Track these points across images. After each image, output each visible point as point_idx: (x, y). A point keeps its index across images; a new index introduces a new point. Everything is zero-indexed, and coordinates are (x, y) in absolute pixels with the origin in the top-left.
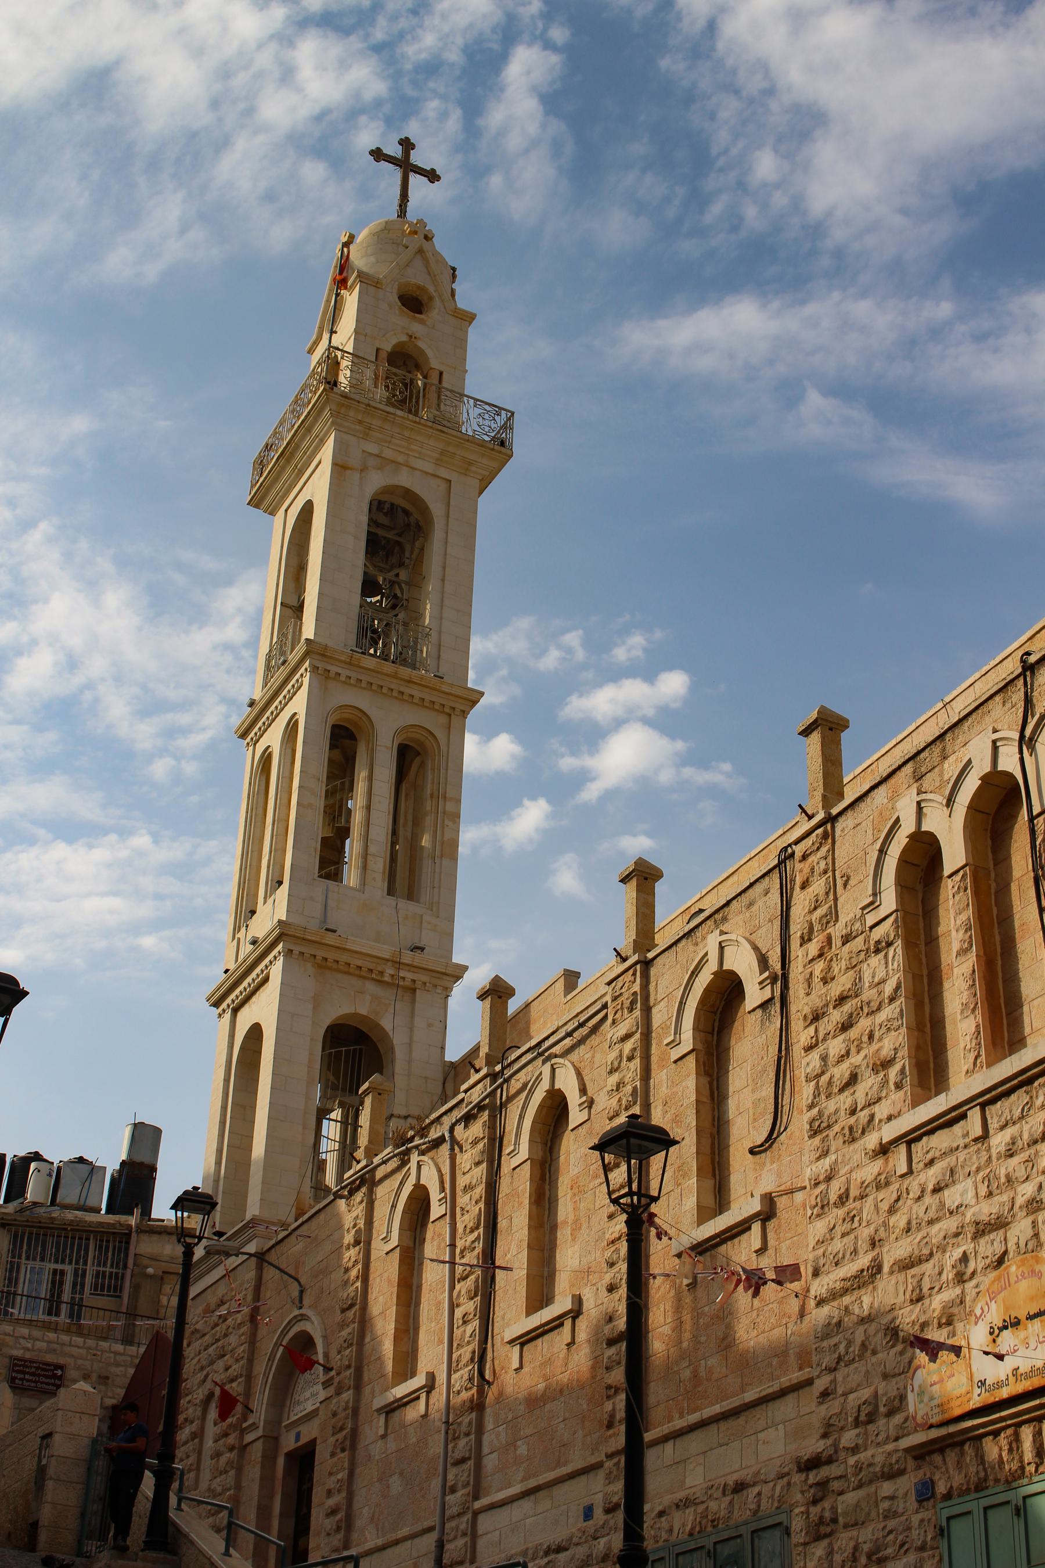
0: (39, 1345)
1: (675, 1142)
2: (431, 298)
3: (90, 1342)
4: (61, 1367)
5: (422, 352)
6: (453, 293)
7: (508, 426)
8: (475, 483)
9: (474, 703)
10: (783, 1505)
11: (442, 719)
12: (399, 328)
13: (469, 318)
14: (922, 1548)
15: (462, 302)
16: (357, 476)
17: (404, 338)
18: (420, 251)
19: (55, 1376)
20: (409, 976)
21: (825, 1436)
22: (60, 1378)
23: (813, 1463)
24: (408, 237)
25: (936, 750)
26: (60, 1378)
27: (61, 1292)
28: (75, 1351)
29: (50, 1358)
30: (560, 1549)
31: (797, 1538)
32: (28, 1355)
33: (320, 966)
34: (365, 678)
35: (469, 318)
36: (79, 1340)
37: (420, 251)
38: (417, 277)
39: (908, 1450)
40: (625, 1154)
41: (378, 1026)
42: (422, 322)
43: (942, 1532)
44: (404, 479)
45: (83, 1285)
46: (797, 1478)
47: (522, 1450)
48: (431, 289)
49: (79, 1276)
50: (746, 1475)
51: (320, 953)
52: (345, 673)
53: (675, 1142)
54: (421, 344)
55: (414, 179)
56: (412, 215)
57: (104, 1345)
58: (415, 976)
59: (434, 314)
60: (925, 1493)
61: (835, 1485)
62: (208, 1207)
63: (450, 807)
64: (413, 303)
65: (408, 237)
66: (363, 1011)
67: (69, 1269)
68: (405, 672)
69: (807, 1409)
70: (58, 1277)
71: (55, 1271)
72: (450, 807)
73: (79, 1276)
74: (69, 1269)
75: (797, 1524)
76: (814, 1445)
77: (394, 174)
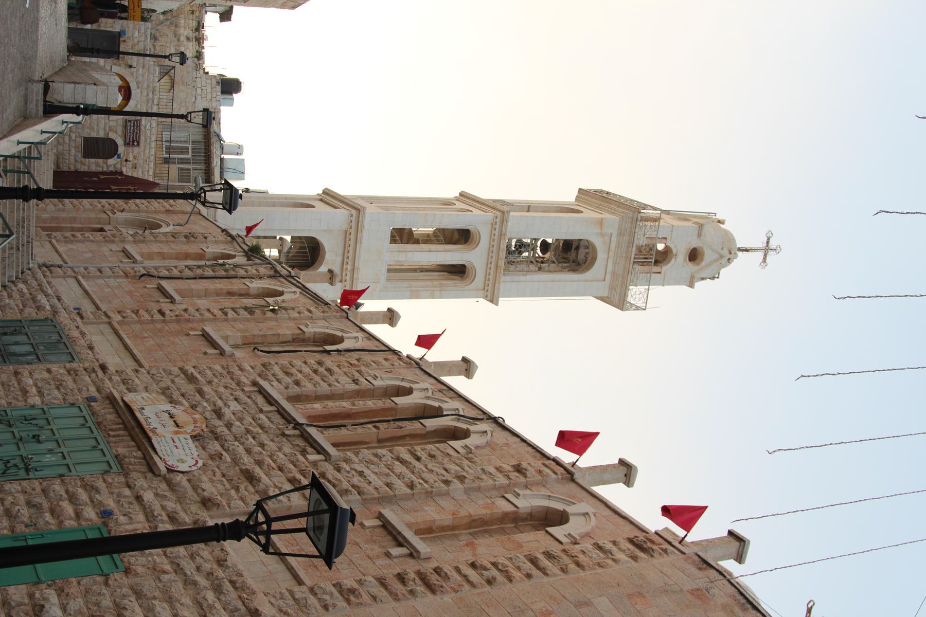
0: (148, 133)
1: (329, 564)
2: (698, 264)
3: (152, 158)
4: (138, 144)
5: (669, 262)
6: (703, 279)
7: (638, 308)
8: (605, 294)
9: (492, 301)
10: (81, 360)
11: (481, 286)
12: (681, 251)
13: (691, 285)
14: (64, 399)
15: (698, 284)
16: (598, 231)
17: (674, 252)
18: (722, 257)
19: (134, 141)
20: (348, 278)
21: (117, 371)
22: (133, 144)
23: (103, 368)
24: (729, 251)
25: (455, 395)
26: (133, 144)
27: (175, 153)
28: (147, 151)
29: (142, 138)
30: (59, 299)
31: (68, 365)
32: (142, 127)
33: (346, 232)
34: (495, 243)
35: (691, 285)
36: (153, 152)
37: (722, 257)
38: (708, 256)
39: (111, 392)
40: (311, 510)
41: (321, 265)
42: (685, 260)
43: (73, 405)
44: (601, 256)
45: (182, 163)
46: (97, 364)
47: (107, 290)
48: (703, 264)
49: (187, 161)
50: (96, 349)
51: (353, 231)
52: (497, 232)
53: (329, 564)
54: (673, 260)
55: (760, 255)
56: (740, 253)
57: (152, 165)
58: (348, 281)
59: (691, 267)
60: (90, 399)
61: (93, 375)
62: (228, 207)
63: (437, 293)
64: (694, 255)
65: (729, 251)
66: (327, 256)
67: (190, 156)
68: (502, 263)
69: (130, 364)
70: (184, 150)
71: (187, 148)
72: (437, 293)
73: (187, 161)
74: (190, 156)
75: (74, 365)
76: (112, 369)
77: (761, 244)
